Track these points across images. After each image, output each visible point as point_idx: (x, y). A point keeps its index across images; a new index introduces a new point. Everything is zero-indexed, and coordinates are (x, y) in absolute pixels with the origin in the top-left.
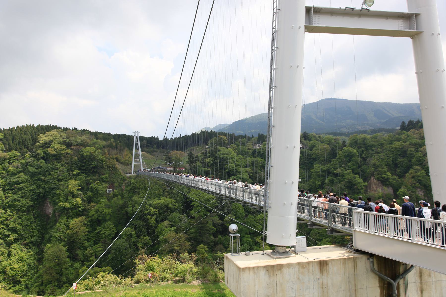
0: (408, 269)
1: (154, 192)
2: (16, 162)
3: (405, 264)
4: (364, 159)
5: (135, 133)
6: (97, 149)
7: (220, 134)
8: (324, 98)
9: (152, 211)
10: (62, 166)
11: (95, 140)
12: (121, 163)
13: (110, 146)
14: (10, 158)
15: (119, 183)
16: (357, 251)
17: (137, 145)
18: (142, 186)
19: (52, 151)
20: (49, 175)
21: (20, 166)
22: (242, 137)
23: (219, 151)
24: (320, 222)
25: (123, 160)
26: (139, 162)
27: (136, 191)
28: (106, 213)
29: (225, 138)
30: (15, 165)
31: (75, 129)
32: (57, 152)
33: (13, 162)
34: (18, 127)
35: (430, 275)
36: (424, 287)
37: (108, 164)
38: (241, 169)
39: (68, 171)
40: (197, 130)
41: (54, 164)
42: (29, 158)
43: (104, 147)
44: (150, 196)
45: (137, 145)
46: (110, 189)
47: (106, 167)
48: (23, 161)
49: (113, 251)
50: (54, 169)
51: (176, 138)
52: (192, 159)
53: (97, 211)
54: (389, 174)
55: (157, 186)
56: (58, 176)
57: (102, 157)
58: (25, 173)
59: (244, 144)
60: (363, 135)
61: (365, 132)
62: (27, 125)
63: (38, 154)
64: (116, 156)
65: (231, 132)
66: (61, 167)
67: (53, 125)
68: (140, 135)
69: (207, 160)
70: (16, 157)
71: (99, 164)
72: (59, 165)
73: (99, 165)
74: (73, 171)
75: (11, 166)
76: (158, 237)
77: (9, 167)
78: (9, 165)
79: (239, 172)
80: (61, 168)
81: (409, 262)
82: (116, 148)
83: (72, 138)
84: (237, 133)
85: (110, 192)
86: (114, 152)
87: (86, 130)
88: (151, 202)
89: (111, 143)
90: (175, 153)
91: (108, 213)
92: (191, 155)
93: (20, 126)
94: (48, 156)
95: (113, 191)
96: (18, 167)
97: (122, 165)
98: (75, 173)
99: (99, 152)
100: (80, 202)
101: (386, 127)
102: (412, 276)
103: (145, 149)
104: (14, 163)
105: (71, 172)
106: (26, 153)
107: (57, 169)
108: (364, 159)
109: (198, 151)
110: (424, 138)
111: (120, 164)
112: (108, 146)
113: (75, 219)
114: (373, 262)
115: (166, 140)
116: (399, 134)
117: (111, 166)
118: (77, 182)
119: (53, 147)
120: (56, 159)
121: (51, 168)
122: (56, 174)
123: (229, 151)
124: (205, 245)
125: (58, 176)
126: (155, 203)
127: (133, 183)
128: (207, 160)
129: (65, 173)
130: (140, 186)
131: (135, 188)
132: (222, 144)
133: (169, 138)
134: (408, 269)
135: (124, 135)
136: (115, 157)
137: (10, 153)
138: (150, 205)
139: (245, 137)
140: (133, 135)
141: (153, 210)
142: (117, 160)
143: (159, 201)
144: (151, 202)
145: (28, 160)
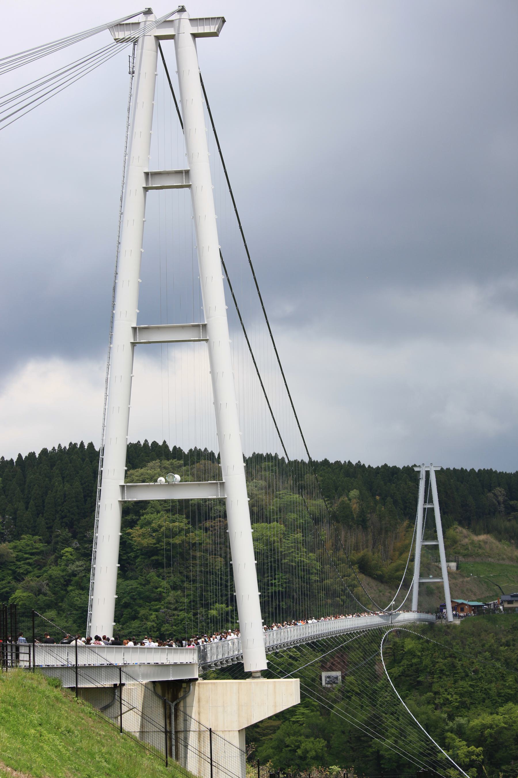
1: (486, 686)
2: (36, 572)
6: (291, 527)
10: (174, 588)
12: (380, 579)
14: (18, 559)
15: (365, 651)
17: (429, 513)
18: (441, 663)
19: (143, 535)
20: (134, 618)
21: (45, 589)
27: (419, 683)
28: (306, 751)
30: (33, 584)
32: (159, 541)
33: (28, 572)
34: (44, 451)
36: (202, 710)
37: (328, 582)
39: (192, 606)
41: (148, 582)
42: (73, 562)
43: (317, 520)
44: (468, 701)
45: (429, 513)
46: (334, 674)
47: (322, 594)
48: (55, 571)
50: (148, 599)
55: (498, 665)
56: (160, 625)
57: (309, 558)
58: (60, 611)
62: (73, 446)
64: (361, 554)
66: (172, 593)
67: (155, 443)
70: (36, 558)
71: (296, 584)
72: (164, 583)
73: (296, 586)
74: (207, 606)
75: (20, 585)
77: (13, 590)
78: (13, 583)
80: (171, 596)
82: (363, 523)
85: (332, 681)
86: (352, 540)
87: (269, 456)
88: (462, 721)
89: (345, 507)
91: (313, 753)
93: (50, 449)
94: (132, 554)
95: (343, 677)
96: (39, 592)
97: (382, 587)
98: (213, 612)
99: (296, 541)
104: (28, 578)
105: (202, 610)
106: (67, 543)
107: (159, 599)
110: (452, 607)
111: (373, 583)
112: (335, 518)
117: (338, 588)
119: (149, 523)
120: (157, 565)
121: (139, 593)
122: (153, 617)
125: (160, 625)
126: (476, 722)
127: (411, 653)
129: (183, 614)
130: (434, 663)
131: (418, 671)
136: (356, 556)
137: (18, 543)
141: (465, 749)
142: (364, 567)
144: (462, 721)
145: (72, 568)
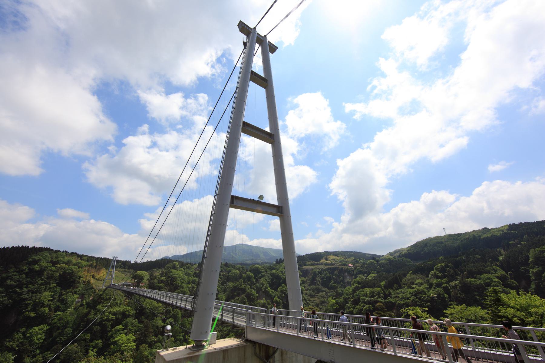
0: (275, 351)
3: (274, 348)
4: (257, 280)
5: (114, 257)
7: (175, 261)
8: (439, 235)
9: (110, 318)
11: (80, 261)
13: (91, 266)
16: (247, 341)
22: (188, 263)
23: (171, 272)
24: (399, 227)
25: (97, 277)
26: (102, 280)
29: (177, 264)
31: (66, 252)
35: (286, 354)
38: (185, 285)
40: (159, 258)
49: (62, 357)
51: (143, 262)
52: (152, 277)
53: (60, 319)
54: (269, 288)
59: (188, 268)
60: (257, 265)
61: (258, 264)
62: (22, 246)
63: (23, 270)
65: (181, 260)
68: (117, 259)
69: (162, 278)
76: (109, 340)
79: (183, 287)
81: (276, 346)
82: (96, 267)
83: (59, 259)
84: (185, 261)
90: (141, 273)
92: (151, 275)
100: (47, 311)
101: (269, 261)
102: (277, 356)
103: (118, 269)
108: (257, 280)
109: (157, 273)
112: (89, 266)
113: (35, 328)
114: (255, 348)
115: (136, 263)
116: (275, 265)
118: (50, 293)
123: (178, 273)
124: (146, 344)
126: (115, 310)
128: (162, 278)
132: (174, 267)
133: (139, 262)
134: (275, 351)
135: (105, 259)
138: (110, 313)
139: (190, 264)
140: (112, 258)
142: (93, 276)
143: (118, 309)
